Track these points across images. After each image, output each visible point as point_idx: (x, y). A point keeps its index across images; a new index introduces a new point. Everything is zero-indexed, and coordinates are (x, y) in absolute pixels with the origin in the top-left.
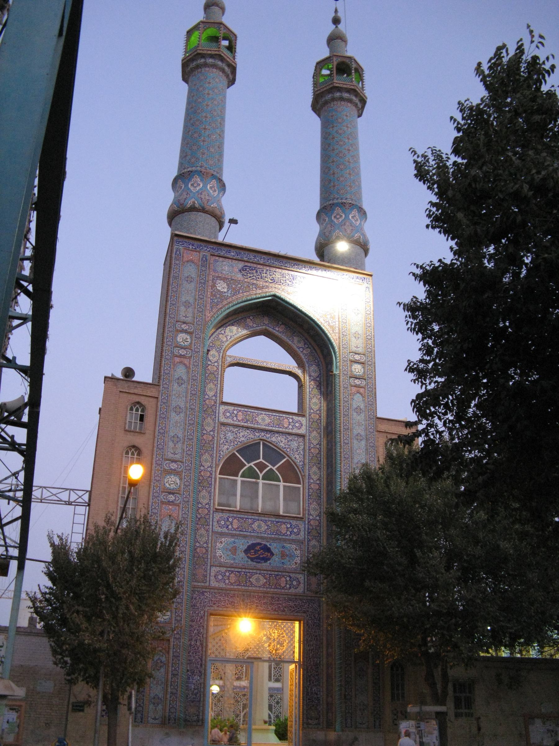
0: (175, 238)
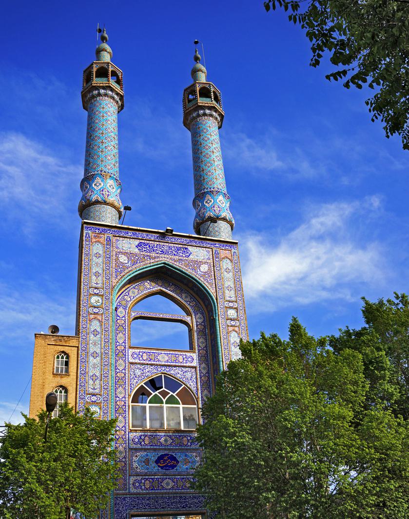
0: (85, 225)
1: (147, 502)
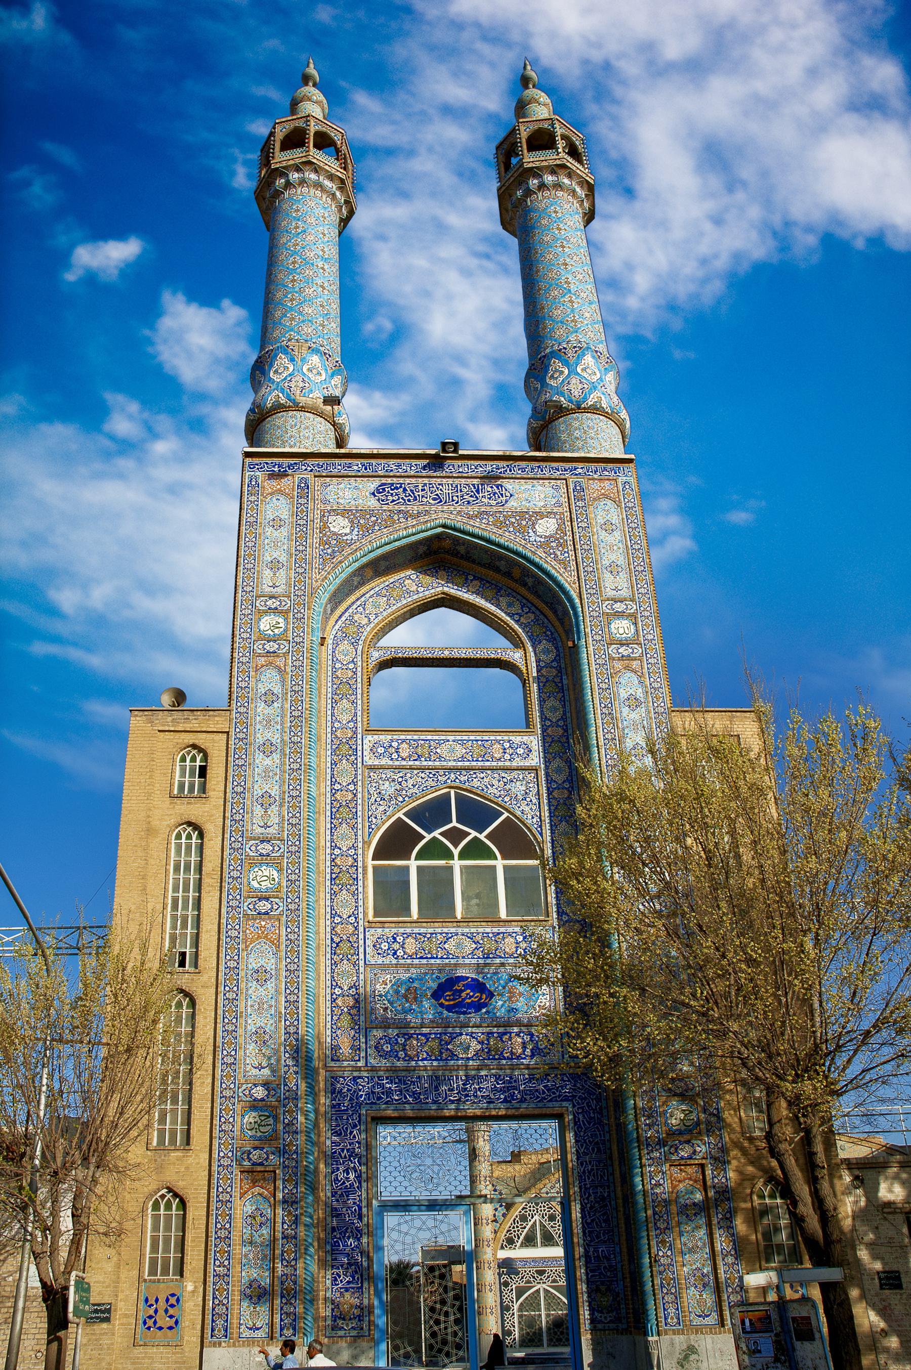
0: (248, 460)
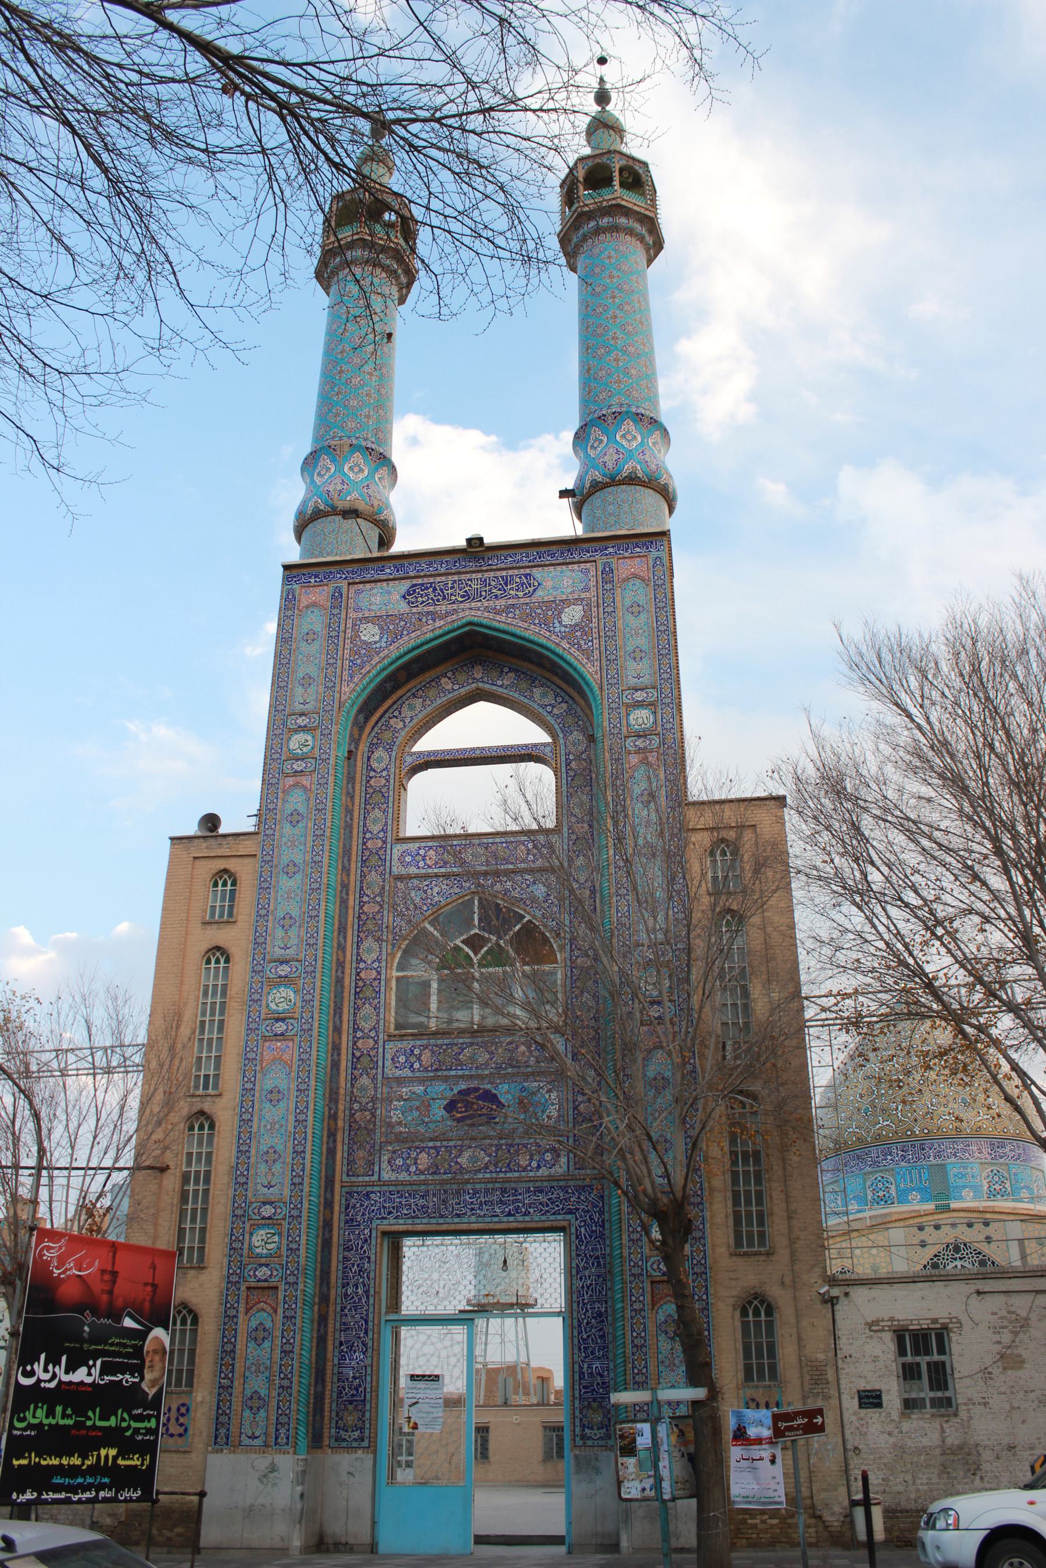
1: (421, 1202)
